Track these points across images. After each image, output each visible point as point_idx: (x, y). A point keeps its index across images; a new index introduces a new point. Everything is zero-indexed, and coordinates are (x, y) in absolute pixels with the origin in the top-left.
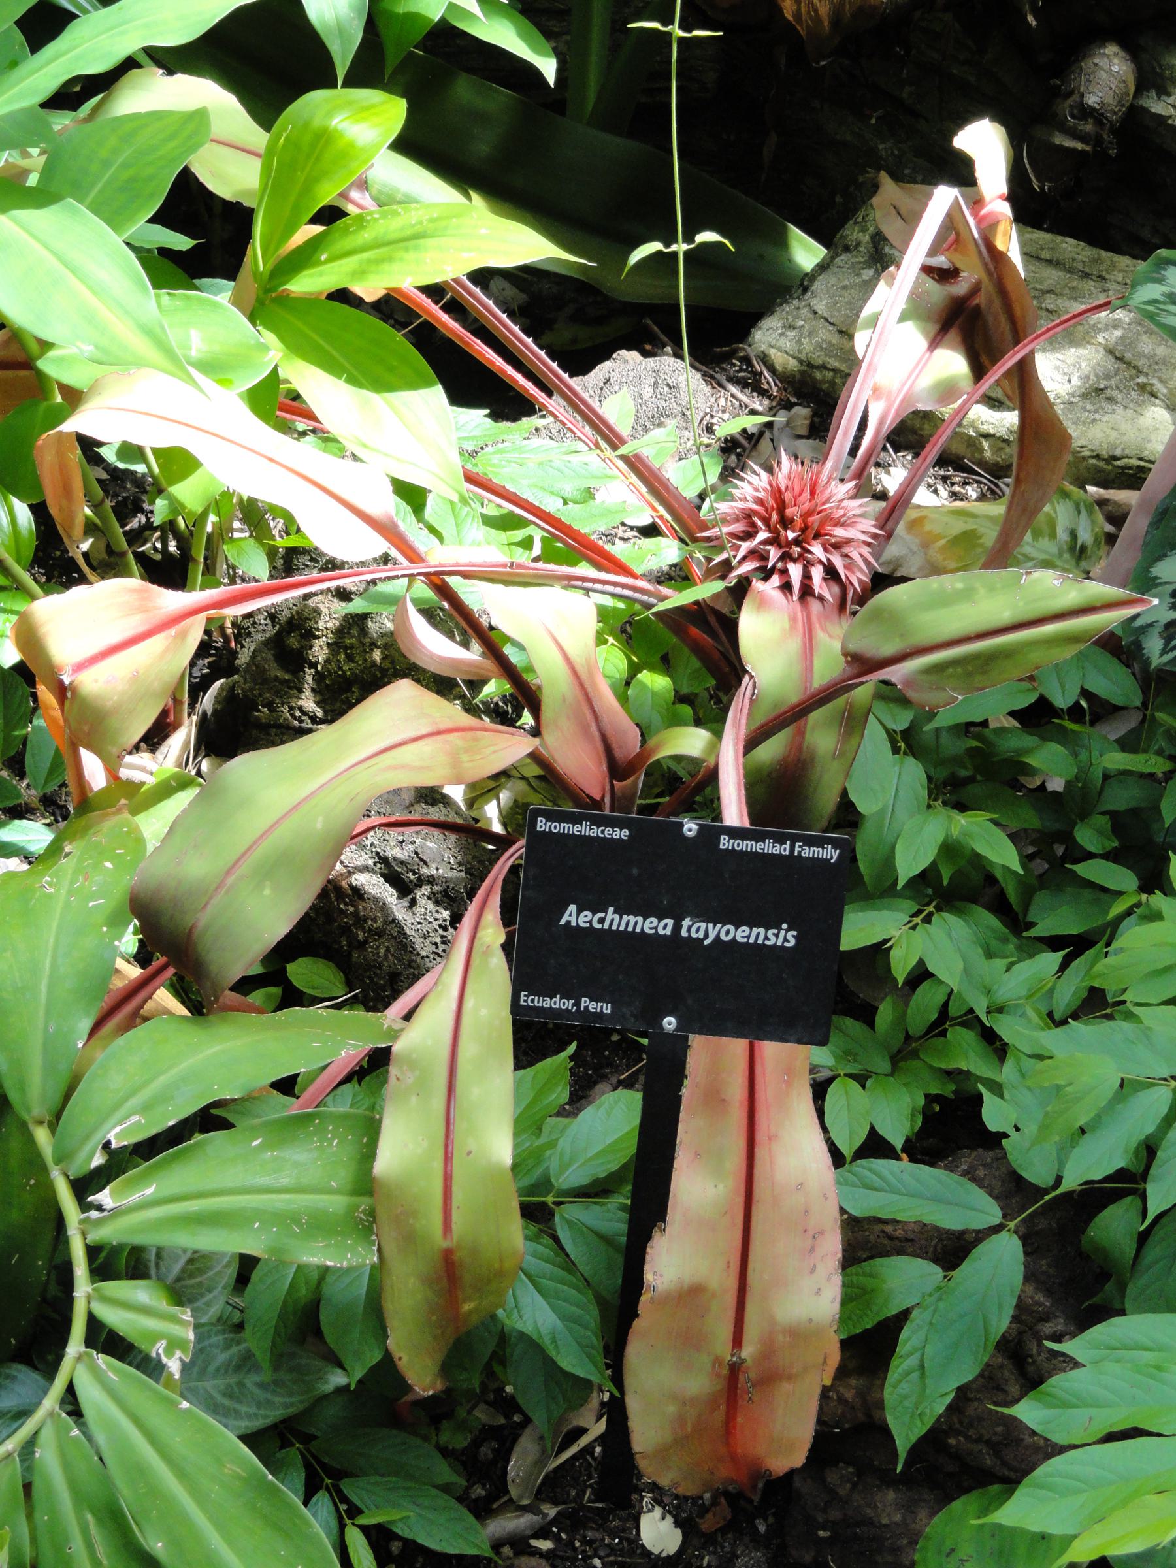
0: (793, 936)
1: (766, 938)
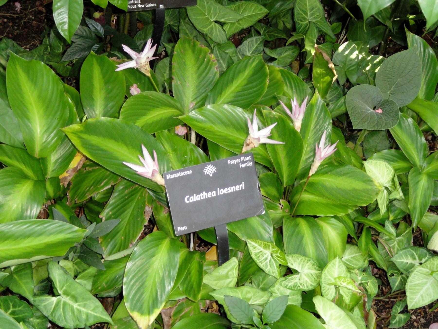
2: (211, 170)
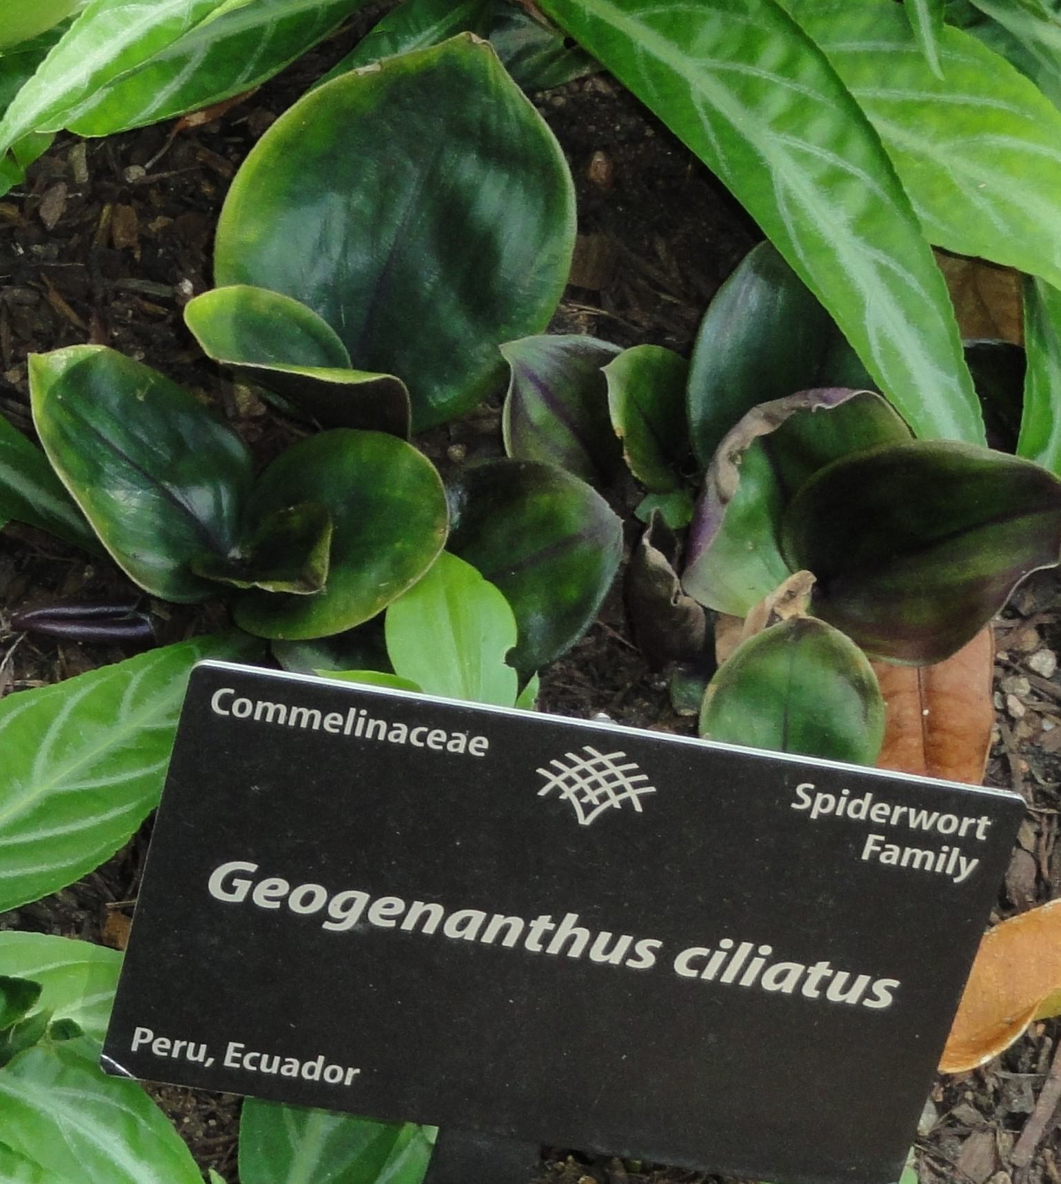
0: (889, 989)
2: (607, 788)
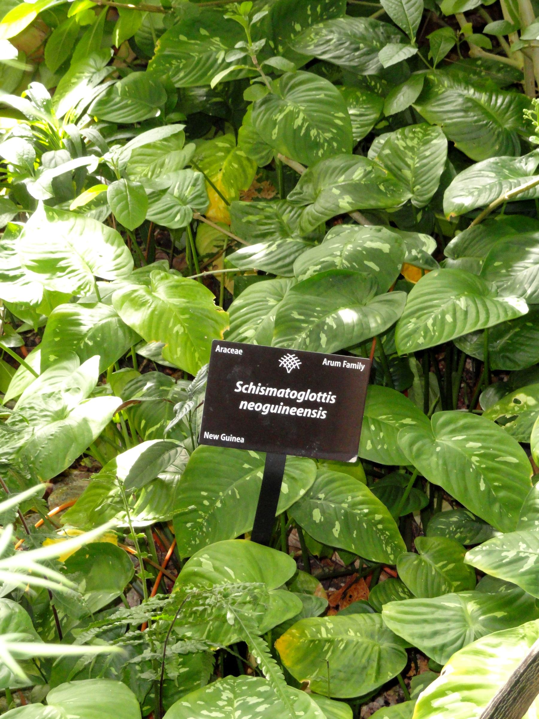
1: (312, 414)
2: (292, 363)
